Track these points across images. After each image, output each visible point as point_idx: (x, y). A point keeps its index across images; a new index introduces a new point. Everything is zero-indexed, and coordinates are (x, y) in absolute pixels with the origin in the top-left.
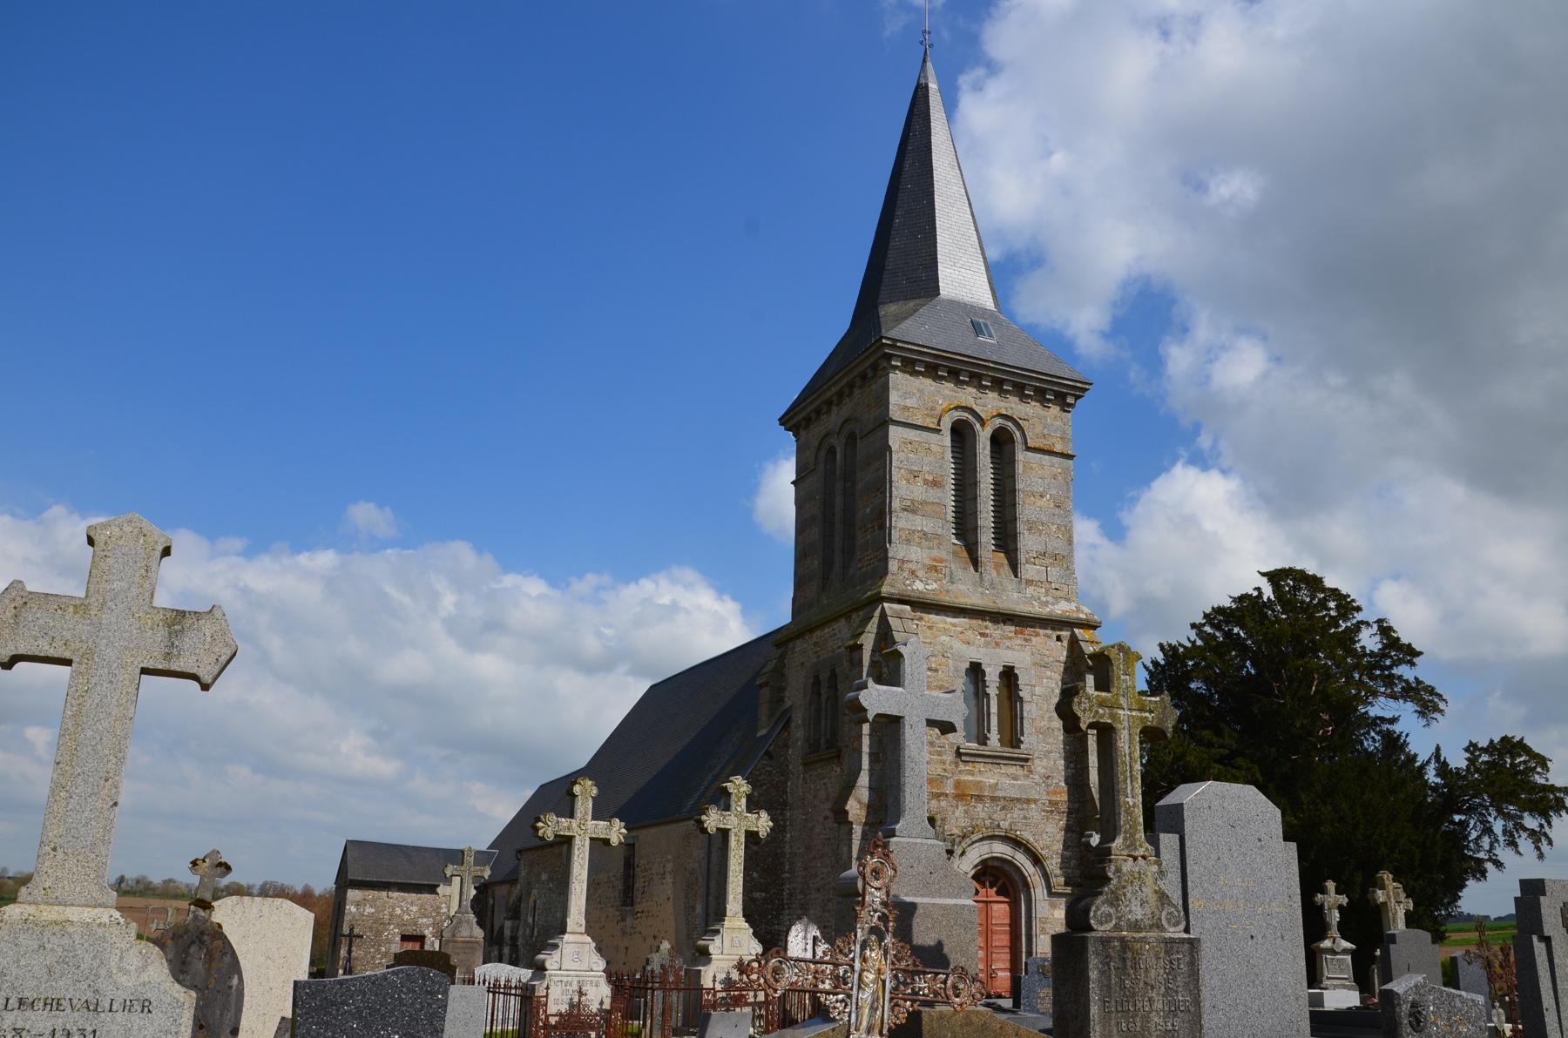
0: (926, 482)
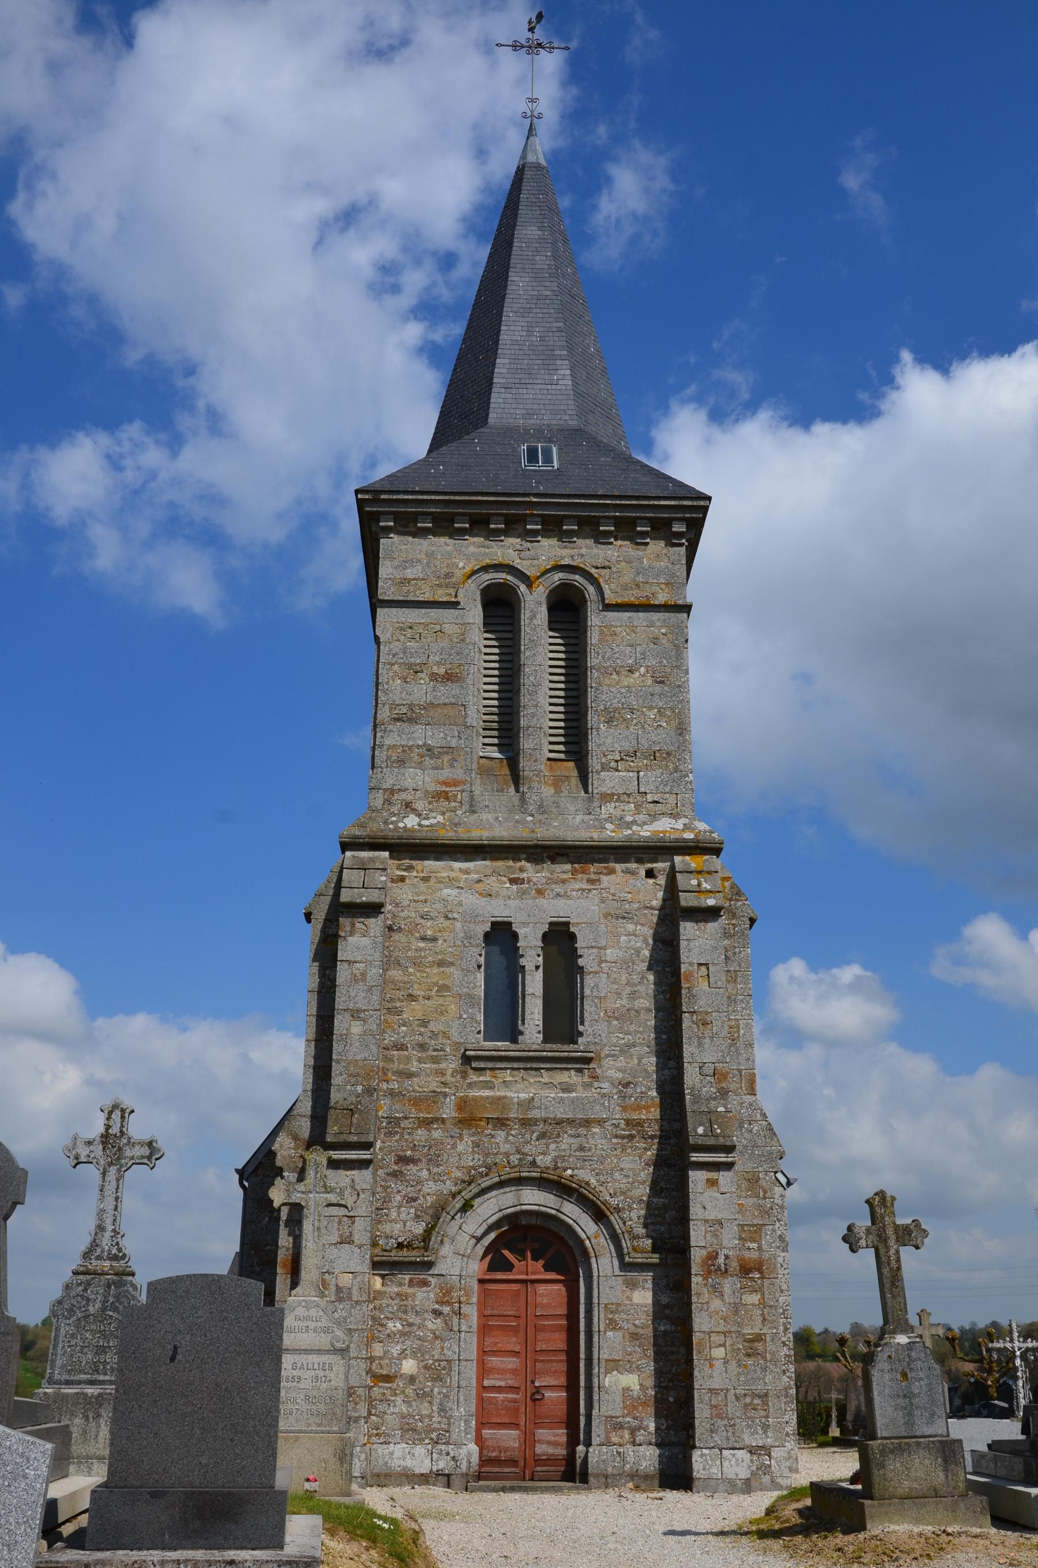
0: (434, 677)
